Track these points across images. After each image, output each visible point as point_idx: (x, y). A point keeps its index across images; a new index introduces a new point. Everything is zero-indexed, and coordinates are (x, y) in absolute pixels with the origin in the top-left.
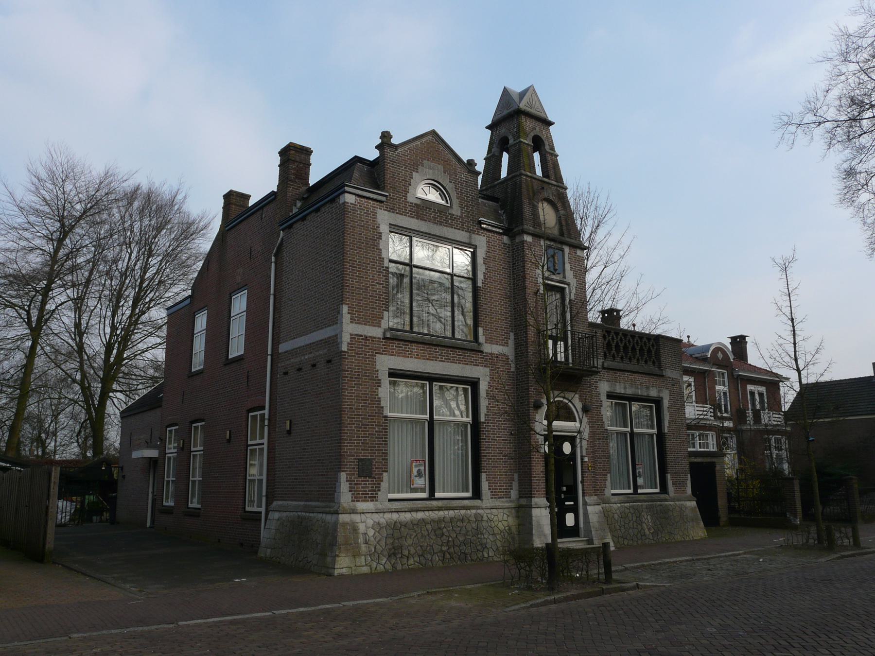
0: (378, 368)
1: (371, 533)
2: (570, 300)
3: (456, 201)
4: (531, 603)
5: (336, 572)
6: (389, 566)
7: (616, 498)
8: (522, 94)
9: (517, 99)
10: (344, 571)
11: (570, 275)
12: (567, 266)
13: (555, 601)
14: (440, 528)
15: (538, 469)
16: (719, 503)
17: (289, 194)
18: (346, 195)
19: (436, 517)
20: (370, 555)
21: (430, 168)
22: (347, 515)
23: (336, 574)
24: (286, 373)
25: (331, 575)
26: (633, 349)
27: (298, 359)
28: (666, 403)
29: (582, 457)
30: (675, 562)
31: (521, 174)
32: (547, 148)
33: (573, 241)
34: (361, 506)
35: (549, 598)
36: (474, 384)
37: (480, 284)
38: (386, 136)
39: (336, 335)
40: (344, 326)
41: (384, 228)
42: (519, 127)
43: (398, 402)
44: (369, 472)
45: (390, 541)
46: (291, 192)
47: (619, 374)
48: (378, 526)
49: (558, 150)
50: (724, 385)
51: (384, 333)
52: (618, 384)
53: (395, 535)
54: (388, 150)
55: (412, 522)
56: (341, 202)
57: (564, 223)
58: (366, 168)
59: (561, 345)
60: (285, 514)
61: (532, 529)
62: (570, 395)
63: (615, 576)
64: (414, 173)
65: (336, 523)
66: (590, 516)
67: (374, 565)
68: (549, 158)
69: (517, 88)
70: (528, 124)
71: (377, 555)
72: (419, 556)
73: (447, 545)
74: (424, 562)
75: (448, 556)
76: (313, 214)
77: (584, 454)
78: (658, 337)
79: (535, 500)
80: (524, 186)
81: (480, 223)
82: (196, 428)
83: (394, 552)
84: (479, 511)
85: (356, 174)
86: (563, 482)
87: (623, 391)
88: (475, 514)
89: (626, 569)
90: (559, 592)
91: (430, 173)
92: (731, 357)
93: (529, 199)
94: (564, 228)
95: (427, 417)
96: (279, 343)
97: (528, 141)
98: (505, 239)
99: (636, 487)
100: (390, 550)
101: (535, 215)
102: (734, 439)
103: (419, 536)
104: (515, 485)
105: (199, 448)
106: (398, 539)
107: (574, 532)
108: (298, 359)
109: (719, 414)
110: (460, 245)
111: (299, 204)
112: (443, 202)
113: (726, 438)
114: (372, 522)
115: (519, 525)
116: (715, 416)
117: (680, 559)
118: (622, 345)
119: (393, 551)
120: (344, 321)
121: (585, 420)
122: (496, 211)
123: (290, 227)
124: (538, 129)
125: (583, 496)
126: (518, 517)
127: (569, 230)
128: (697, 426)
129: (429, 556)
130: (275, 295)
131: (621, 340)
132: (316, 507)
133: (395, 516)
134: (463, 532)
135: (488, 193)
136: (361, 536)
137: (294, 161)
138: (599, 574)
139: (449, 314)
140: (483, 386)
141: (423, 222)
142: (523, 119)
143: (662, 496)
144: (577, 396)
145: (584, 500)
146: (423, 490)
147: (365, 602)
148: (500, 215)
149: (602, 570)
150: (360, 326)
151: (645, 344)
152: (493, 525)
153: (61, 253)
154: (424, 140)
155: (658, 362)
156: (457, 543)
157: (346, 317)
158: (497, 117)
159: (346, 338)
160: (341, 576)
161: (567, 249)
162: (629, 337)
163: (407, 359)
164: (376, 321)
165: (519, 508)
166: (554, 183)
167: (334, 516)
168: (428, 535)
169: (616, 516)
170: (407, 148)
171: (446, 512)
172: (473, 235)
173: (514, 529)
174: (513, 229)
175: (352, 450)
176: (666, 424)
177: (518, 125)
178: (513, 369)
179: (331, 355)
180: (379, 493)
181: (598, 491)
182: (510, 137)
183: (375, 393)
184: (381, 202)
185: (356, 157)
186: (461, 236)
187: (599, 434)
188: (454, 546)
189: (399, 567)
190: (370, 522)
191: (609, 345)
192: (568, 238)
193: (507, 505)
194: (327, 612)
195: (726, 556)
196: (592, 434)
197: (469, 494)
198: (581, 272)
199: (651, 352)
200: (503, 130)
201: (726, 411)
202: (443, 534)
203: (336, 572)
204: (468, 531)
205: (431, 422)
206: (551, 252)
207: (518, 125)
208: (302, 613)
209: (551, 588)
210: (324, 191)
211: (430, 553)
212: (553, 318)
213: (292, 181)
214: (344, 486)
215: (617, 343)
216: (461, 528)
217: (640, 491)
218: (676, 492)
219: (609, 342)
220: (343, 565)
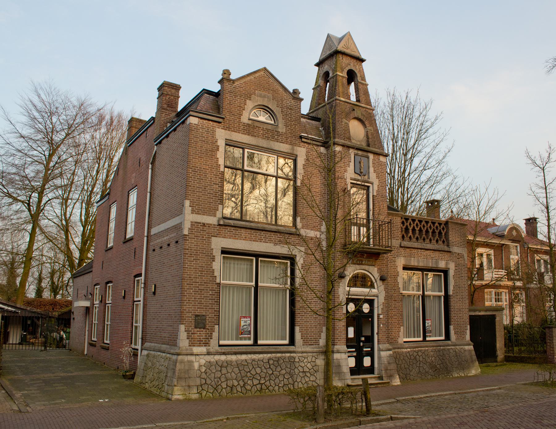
7: (407, 345)
8: (341, 40)
9: (336, 43)
12: (372, 170)
18: (191, 117)
20: (201, 386)
26: (427, 232)
28: (451, 273)
29: (378, 315)
32: (359, 79)
34: (196, 350)
36: (292, 259)
38: (226, 73)
51: (219, 221)
54: (226, 84)
59: (363, 230)
62: (371, 268)
68: (360, 86)
70: (344, 61)
77: (380, 312)
79: (336, 347)
81: (301, 137)
82: (109, 286)
84: (292, 355)
87: (416, 264)
89: (398, 401)
95: (253, 283)
98: (322, 149)
101: (347, 130)
105: (110, 302)
107: (371, 370)
110: (285, 155)
114: (204, 362)
120: (186, 212)
121: (382, 288)
125: (378, 344)
131: (417, 225)
133: (223, 358)
135: (313, 115)
145: (379, 347)
148: (321, 131)
150: (199, 216)
151: (437, 227)
153: (52, 164)
154: (257, 75)
155: (446, 242)
161: (371, 156)
163: (236, 241)
170: (242, 81)
172: (295, 147)
177: (339, 65)
180: (211, 340)
184: (219, 123)
185: (204, 90)
186: (284, 147)
190: (203, 362)
196: (387, 298)
206: (358, 158)
207: (339, 65)
214: (183, 335)
215: (414, 227)
219: (407, 226)
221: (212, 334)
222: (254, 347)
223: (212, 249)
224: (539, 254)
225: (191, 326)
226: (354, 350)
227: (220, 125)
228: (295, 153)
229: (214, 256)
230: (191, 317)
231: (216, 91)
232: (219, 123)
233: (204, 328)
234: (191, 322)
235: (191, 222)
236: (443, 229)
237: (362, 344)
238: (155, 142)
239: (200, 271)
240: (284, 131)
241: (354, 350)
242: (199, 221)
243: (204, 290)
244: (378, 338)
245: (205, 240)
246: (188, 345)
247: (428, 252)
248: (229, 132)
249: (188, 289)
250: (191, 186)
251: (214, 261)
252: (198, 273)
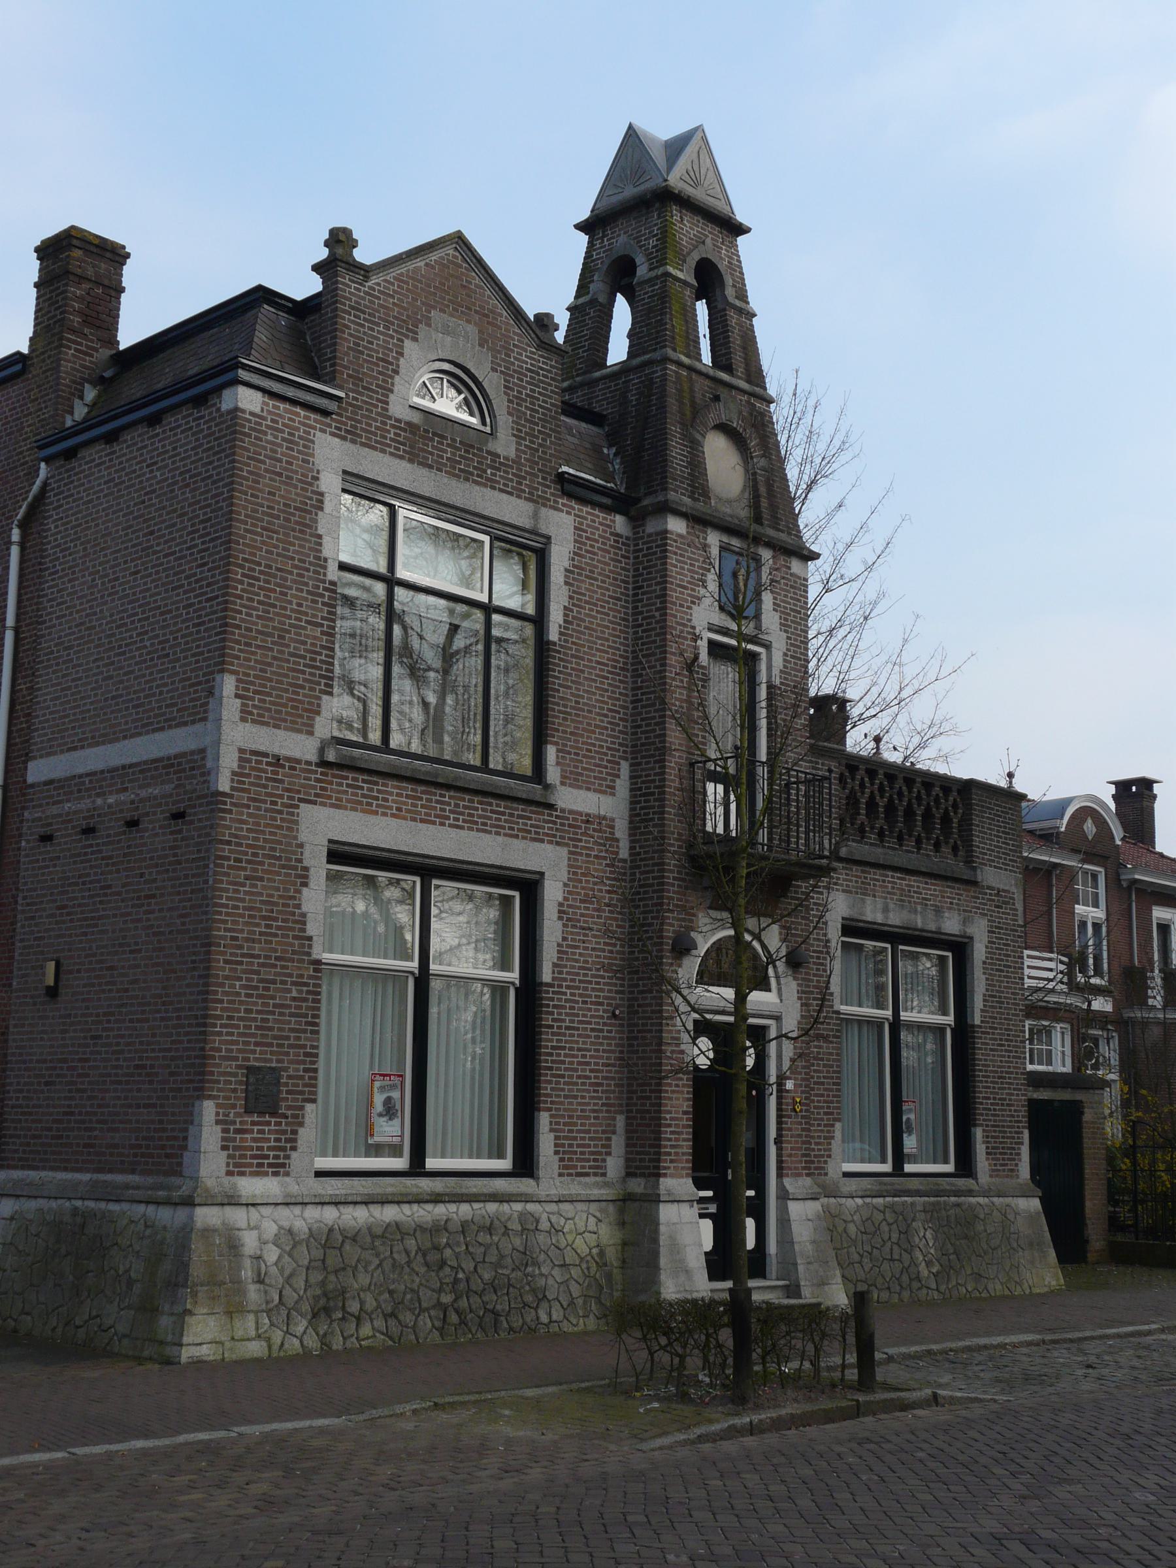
0: (303, 836)
1: (272, 1255)
2: (770, 687)
3: (504, 421)
4: (698, 1431)
5: (186, 1354)
6: (312, 1342)
7: (852, 1185)
8: (676, 147)
10: (205, 1352)
11: (770, 619)
13: (752, 1430)
14: (436, 1248)
15: (678, 1103)
16: (1088, 1204)
17: (66, 366)
18: (242, 391)
19: (429, 1218)
20: (269, 1312)
21: (446, 331)
22: (214, 1210)
23: (184, 1359)
24: (46, 838)
25: (169, 1362)
26: (909, 813)
27: (84, 804)
28: (979, 951)
30: (1003, 1346)
31: (666, 359)
32: (730, 292)
33: (783, 536)
34: (251, 1186)
35: (737, 1421)
36: (529, 886)
37: (553, 635)
38: (340, 240)
39: (202, 751)
40: (226, 727)
41: (330, 482)
42: (665, 236)
43: (347, 926)
44: (271, 1100)
45: (316, 1277)
46: (72, 360)
47: (876, 874)
48: (288, 1238)
49: (755, 301)
50: (1096, 905)
51: (322, 751)
52: (869, 900)
53: (329, 1262)
55: (369, 1229)
56: (226, 406)
57: (763, 490)
58: (283, 319)
60: (33, 1204)
61: (656, 1254)
63: (880, 1374)
64: (408, 344)
65: (186, 1230)
66: (795, 1227)
67: (277, 1336)
68: (733, 319)
69: (661, 129)
70: (686, 228)
71: (284, 1313)
72: (386, 1316)
73: (454, 1290)
74: (395, 1329)
75: (454, 1318)
76: (141, 429)
78: (969, 787)
80: (671, 390)
83: (327, 1305)
84: (531, 1207)
85: (261, 336)
86: (726, 1136)
87: (879, 918)
88: (522, 1216)
90: (758, 1407)
91: (447, 346)
92: (1118, 833)
93: (683, 425)
94: (764, 503)
96: (27, 757)
97: (685, 274)
98: (620, 523)
99: (899, 1158)
100: (316, 1298)
101: (696, 464)
102: (1115, 1044)
103: (387, 1265)
104: (618, 1143)
106: (336, 1272)
108: (84, 804)
109: (1080, 978)
111: (90, 394)
112: (474, 421)
113: (1096, 1041)
115: (625, 1244)
116: (1074, 987)
117: (1014, 1339)
118: (882, 803)
119: (322, 1302)
120: (225, 714)
122: (597, 449)
123: (70, 454)
124: (711, 243)
125: (780, 1175)
126: (622, 1224)
127: (773, 507)
128: (1041, 1010)
129: (408, 1318)
130: (17, 630)
132: (127, 1186)
133: (330, 1214)
134: (492, 1257)
135: (577, 399)
136: (247, 1263)
137: (82, 278)
138: (844, 1366)
139: (376, 672)
140: (552, 893)
141: (424, 471)
142: (675, 214)
143: (961, 1182)
144: (775, 928)
145: (782, 1189)
146: (394, 1150)
147: (290, 1425)
148: (605, 459)
149: (852, 1359)
150: (264, 730)
151: (937, 800)
152: (563, 1244)
154: (434, 257)
155: (964, 848)
156: (477, 1284)
157: (231, 707)
159: (228, 761)
160: (198, 1364)
161: (766, 554)
162: (899, 783)
163: (372, 819)
164: (301, 718)
165: (626, 1200)
166: (743, 384)
167: (181, 1213)
168: (409, 1263)
169: (852, 1229)
170: (392, 274)
171: (452, 1207)
172: (543, 510)
173: (612, 1255)
174: (639, 500)
175: (232, 1045)
176: (978, 1002)
177: (659, 226)
178: (624, 853)
179: (186, 801)
180: (294, 1155)
181: (814, 1166)
182: (640, 259)
183: (292, 901)
184: (326, 413)
185: (260, 288)
187: (819, 1020)
188: (469, 1291)
189: (337, 1343)
191: (852, 801)
192: (767, 528)
193: (596, 1193)
194: (206, 1448)
195: (1119, 1336)
197: (504, 1164)
198: (796, 617)
199: (937, 817)
200: (623, 239)
201: (1098, 972)
202: (443, 1263)
203: (186, 1354)
204: (502, 1257)
205: (423, 979)
207: (659, 226)
208: (145, 1452)
209: (738, 1394)
210: (165, 373)
211: (412, 1310)
212: (724, 731)
213: (73, 331)
214: (209, 1136)
216: (487, 1247)
217: (909, 1168)
218: (994, 1173)
219: (852, 791)
220: (204, 1336)
221: (295, 1132)
222: (409, 1182)
223: (301, 846)
225: (234, 1106)
226: (710, 1193)
227: (328, 420)
228: (543, 530)
229: (306, 869)
230: (235, 1075)
231: (299, 295)
232: (326, 413)
233: (273, 1114)
234: (234, 1091)
235: (241, 751)
236: (955, 806)
238: (40, 448)
239: (264, 918)
240: (512, 454)
241: (710, 1193)
242: (262, 748)
243: (274, 982)
244: (779, 1155)
245: (280, 812)
246: (224, 1169)
247: (913, 880)
248: (352, 446)
249: (227, 978)
250: (239, 627)
251: (305, 885)
252: (258, 925)
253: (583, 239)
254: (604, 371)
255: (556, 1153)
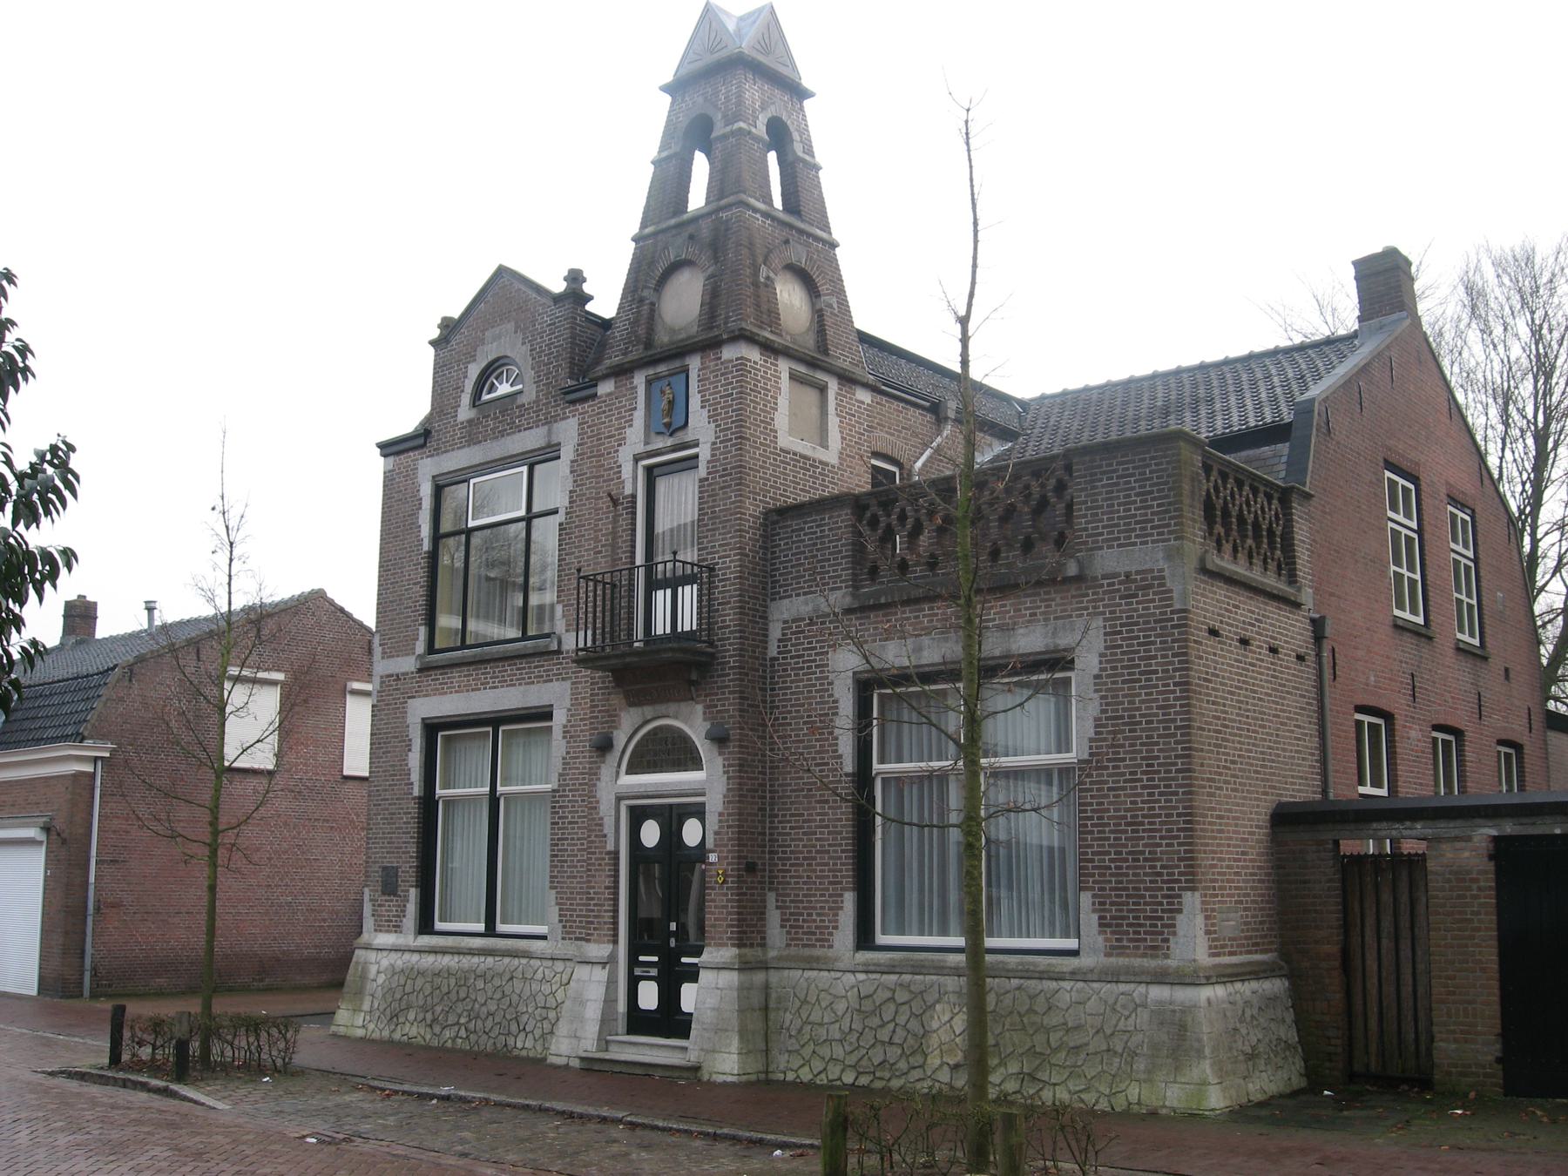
12: (695, 401)
48: (393, 971)
70: (753, 92)
97: (761, 130)
158: (683, 72)
190: (385, 963)
205: (494, 799)
224: (810, 514)
226: (655, 959)
237: (673, 943)
241: (655, 959)
253: (667, 99)
254: (685, 217)
255: (836, 701)
